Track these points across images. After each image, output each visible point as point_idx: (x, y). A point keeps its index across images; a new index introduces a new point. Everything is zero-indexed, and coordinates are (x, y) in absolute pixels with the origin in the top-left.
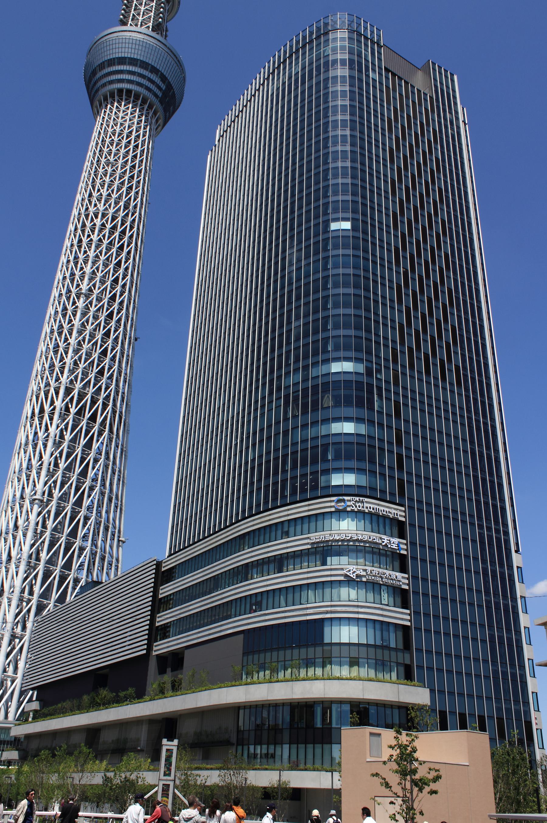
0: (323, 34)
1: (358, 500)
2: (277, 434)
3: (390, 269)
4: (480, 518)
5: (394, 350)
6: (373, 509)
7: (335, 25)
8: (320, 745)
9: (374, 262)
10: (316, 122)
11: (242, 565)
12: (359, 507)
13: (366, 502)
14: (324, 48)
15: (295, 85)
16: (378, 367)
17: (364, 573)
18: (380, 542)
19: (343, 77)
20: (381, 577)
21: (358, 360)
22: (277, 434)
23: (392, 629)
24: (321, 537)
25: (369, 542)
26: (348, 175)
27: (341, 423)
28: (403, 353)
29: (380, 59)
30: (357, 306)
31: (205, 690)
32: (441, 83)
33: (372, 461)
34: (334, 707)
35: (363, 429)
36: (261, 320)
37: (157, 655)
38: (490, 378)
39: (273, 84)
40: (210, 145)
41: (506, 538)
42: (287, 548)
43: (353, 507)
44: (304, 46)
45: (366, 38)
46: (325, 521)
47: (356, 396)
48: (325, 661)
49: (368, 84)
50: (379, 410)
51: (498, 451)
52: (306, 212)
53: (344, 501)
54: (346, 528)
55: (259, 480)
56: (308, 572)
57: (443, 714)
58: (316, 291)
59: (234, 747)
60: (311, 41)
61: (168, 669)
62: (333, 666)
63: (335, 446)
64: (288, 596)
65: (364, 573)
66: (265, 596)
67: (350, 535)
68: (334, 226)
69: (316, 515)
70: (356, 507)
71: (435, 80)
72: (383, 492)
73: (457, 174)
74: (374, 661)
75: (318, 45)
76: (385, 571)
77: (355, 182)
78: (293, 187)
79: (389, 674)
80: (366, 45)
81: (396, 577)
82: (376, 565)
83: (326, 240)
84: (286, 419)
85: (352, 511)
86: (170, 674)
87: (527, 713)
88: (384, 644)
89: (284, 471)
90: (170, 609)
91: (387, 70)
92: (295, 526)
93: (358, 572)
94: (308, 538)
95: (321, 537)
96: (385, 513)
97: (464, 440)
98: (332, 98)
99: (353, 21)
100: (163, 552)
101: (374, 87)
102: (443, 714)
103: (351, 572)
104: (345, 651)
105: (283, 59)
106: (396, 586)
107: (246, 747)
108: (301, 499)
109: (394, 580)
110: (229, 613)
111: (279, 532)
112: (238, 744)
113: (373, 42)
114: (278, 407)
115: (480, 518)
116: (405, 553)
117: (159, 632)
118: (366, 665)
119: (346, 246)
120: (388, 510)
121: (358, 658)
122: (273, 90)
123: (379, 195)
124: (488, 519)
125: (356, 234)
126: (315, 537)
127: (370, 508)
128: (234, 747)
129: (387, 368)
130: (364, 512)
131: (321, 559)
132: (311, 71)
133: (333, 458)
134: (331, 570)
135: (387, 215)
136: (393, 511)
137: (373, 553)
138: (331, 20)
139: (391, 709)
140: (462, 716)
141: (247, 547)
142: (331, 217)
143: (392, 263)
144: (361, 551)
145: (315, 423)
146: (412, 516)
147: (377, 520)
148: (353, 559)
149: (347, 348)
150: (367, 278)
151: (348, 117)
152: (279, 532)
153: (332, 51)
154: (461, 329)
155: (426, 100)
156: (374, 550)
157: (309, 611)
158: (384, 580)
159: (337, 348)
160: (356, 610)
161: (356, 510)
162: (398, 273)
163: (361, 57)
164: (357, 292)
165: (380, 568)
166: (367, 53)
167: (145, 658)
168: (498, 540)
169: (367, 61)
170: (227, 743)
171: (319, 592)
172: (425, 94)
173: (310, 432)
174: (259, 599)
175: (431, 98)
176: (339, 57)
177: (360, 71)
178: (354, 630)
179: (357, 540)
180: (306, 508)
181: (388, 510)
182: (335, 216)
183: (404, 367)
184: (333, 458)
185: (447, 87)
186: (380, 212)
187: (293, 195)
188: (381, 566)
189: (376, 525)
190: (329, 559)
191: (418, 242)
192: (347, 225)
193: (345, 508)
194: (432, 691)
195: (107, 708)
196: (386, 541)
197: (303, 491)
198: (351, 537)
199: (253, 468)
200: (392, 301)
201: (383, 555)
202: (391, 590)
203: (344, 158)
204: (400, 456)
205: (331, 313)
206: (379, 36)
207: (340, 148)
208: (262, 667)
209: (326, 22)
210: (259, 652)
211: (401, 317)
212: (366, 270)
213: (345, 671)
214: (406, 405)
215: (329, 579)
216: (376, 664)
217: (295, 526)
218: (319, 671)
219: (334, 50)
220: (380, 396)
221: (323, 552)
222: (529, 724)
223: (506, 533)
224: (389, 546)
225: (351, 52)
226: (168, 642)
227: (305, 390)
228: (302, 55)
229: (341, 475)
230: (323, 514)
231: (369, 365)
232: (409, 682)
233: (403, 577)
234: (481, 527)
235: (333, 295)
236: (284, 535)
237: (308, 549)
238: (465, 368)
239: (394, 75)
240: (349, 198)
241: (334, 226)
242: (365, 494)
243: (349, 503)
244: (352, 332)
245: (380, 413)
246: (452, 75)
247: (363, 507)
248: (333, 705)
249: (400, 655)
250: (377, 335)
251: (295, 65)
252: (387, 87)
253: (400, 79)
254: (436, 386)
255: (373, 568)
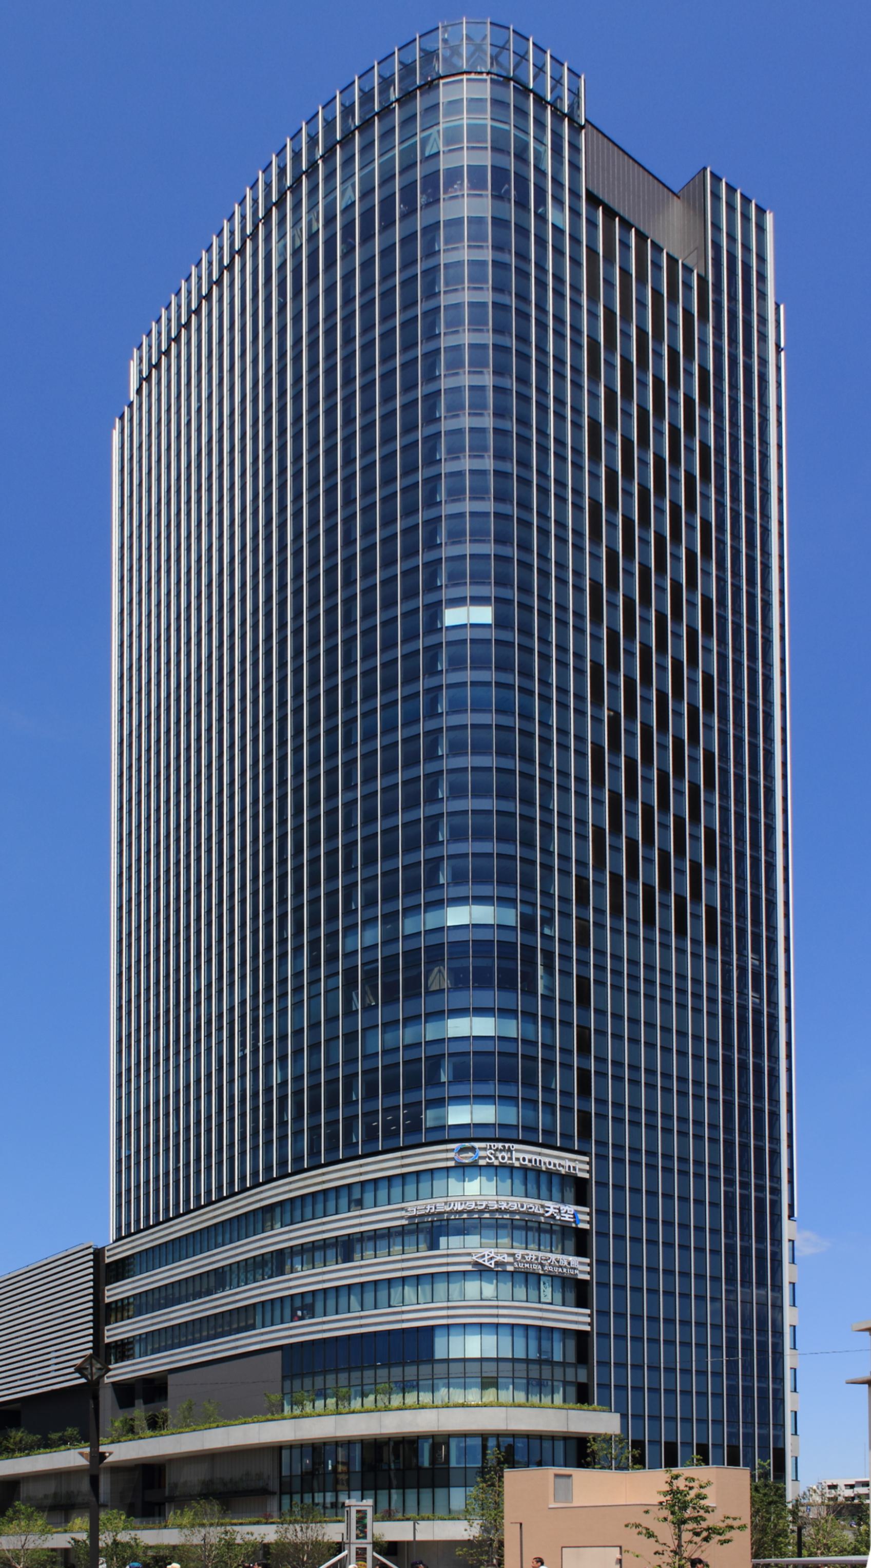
0: (418, 85)
1: (500, 1147)
2: (331, 1040)
3: (579, 548)
4: (729, 1168)
5: (582, 881)
6: (530, 1161)
7: (455, 60)
8: (429, 1490)
9: (545, 699)
10: (404, 308)
11: (272, 1252)
12: (503, 1158)
13: (516, 1150)
14: (423, 130)
15: (343, 241)
16: (547, 914)
17: (511, 1260)
18: (541, 1211)
19: (476, 221)
20: (541, 1264)
21: (506, 901)
22: (331, 1040)
23: (556, 1336)
24: (429, 1207)
25: (520, 1213)
26: (486, 449)
27: (468, 1019)
28: (599, 884)
29: (575, 167)
30: (505, 751)
31: (217, 1427)
32: (731, 238)
33: (530, 1083)
34: (453, 1443)
35: (512, 1028)
36: (282, 743)
37: (113, 1383)
38: (776, 928)
39: (282, 236)
40: (116, 406)
41: (775, 1198)
42: (361, 1224)
43: (490, 1159)
44: (366, 124)
45: (540, 101)
46: (434, 1182)
47: (497, 967)
48: (438, 1384)
49: (541, 242)
50: (547, 993)
51: (777, 1058)
52: (383, 418)
53: (473, 1149)
54: (475, 1192)
55: (298, 1117)
56: (403, 1261)
57: (638, 1444)
58: (410, 552)
59: (276, 1497)
60: (386, 111)
61: (136, 1402)
62: (451, 1389)
63: (454, 862)
64: (365, 1295)
65: (511, 1260)
66: (320, 1297)
67: (484, 1204)
68: (452, 617)
69: (418, 1173)
70: (497, 1158)
71: (716, 227)
72: (549, 1132)
73: (750, 485)
74: (525, 1381)
75: (408, 121)
76: (549, 1255)
77: (504, 508)
78: (349, 358)
79: (550, 1397)
80: (540, 124)
81: (569, 1264)
82: (531, 1246)
83: (433, 651)
84: (350, 1013)
85: (489, 1165)
86: (143, 1406)
87: (780, 1437)
88: (543, 1357)
89: (350, 1102)
90: (129, 1318)
91: (594, 200)
92: (375, 1190)
93: (499, 1258)
94: (402, 1209)
95: (429, 1207)
96: (552, 1167)
97: (712, 1042)
98: (447, 284)
99: (504, 48)
100: (103, 1231)
101: (559, 252)
102: (638, 1444)
103: (486, 1258)
104: (473, 1368)
105: (308, 160)
106: (568, 1275)
107: (297, 1498)
108: (385, 1148)
109: (565, 1267)
110: (251, 1322)
111: (344, 1202)
112: (282, 1493)
113: (558, 115)
114: (331, 991)
115: (729, 1168)
116: (587, 1226)
117: (113, 1351)
118: (511, 1387)
119: (480, 663)
120: (557, 1162)
121: (497, 1378)
122: (282, 253)
123: (561, 458)
124: (745, 1171)
125: (505, 636)
126: (415, 1207)
127: (524, 1159)
128: (276, 1497)
129: (565, 915)
130: (512, 1168)
131: (428, 1241)
132: (387, 203)
133: (451, 1079)
134: (448, 1255)
135: (577, 345)
136: (567, 1163)
137: (527, 1228)
138: (445, 41)
139: (551, 1442)
140: (671, 1449)
141: (279, 1225)
142: (445, 594)
143: (584, 699)
144: (504, 1226)
145: (412, 1019)
146: (602, 1170)
147: (536, 1179)
148: (489, 1239)
149: (482, 877)
150: (527, 734)
151: (488, 255)
152: (344, 1202)
153: (448, 142)
154: (725, 834)
155: (688, 286)
156: (529, 1224)
157: (405, 1317)
158: (546, 1268)
159: (458, 878)
160: (494, 1311)
161: (496, 1163)
162: (597, 720)
163: (526, 162)
164: (506, 763)
165: (539, 1250)
166: (541, 149)
167: (90, 1390)
168: (760, 1202)
169: (540, 172)
170: (265, 1492)
171: (425, 1289)
172: (688, 270)
173: (404, 1036)
174: (309, 1300)
175: (702, 280)
176: (465, 159)
177: (522, 204)
178: (490, 1340)
179: (498, 1210)
180: (398, 1163)
181: (557, 1162)
182: (456, 592)
183: (599, 911)
184: (451, 1079)
185: (746, 248)
186: (560, 417)
187: (348, 339)
188: (542, 1248)
189: (535, 1186)
190: (443, 1240)
191: (644, 491)
192: (484, 615)
193: (476, 1161)
194: (624, 1416)
195: (28, 1455)
196: (551, 1211)
197: (390, 1134)
198: (487, 1206)
199: (282, 1099)
200: (581, 780)
201: (545, 1231)
202: (558, 1282)
203: (478, 451)
204: (584, 1075)
205: (445, 680)
206: (574, 93)
207: (466, 464)
208: (323, 1394)
209: (429, 47)
210: (314, 1374)
211: (595, 569)
212: (526, 716)
213: (473, 1395)
214: (600, 983)
215: (444, 1269)
216: (528, 1383)
217: (375, 1190)
218: (426, 1397)
219: (453, 136)
220: (549, 968)
221: (432, 1230)
222: (780, 1455)
223: (776, 1191)
224: (558, 1218)
225: (498, 149)
226: (134, 1282)
227: (390, 961)
228: (363, 150)
229: (469, 1107)
230: (432, 1171)
231: (528, 910)
232: (585, 1406)
233: (580, 1263)
234: (730, 1182)
235: (450, 517)
236: (353, 1204)
237: (403, 1226)
238: (726, 911)
239: (610, 213)
240: (490, 506)
241: (452, 617)
242: (516, 1138)
243: (482, 1153)
244: (492, 761)
245: (548, 998)
246: (761, 211)
247: (510, 1159)
248: (451, 1439)
249: (570, 1372)
250: (546, 809)
251: (342, 183)
252: (592, 252)
253: (626, 225)
254: (665, 946)
255: (527, 1252)
